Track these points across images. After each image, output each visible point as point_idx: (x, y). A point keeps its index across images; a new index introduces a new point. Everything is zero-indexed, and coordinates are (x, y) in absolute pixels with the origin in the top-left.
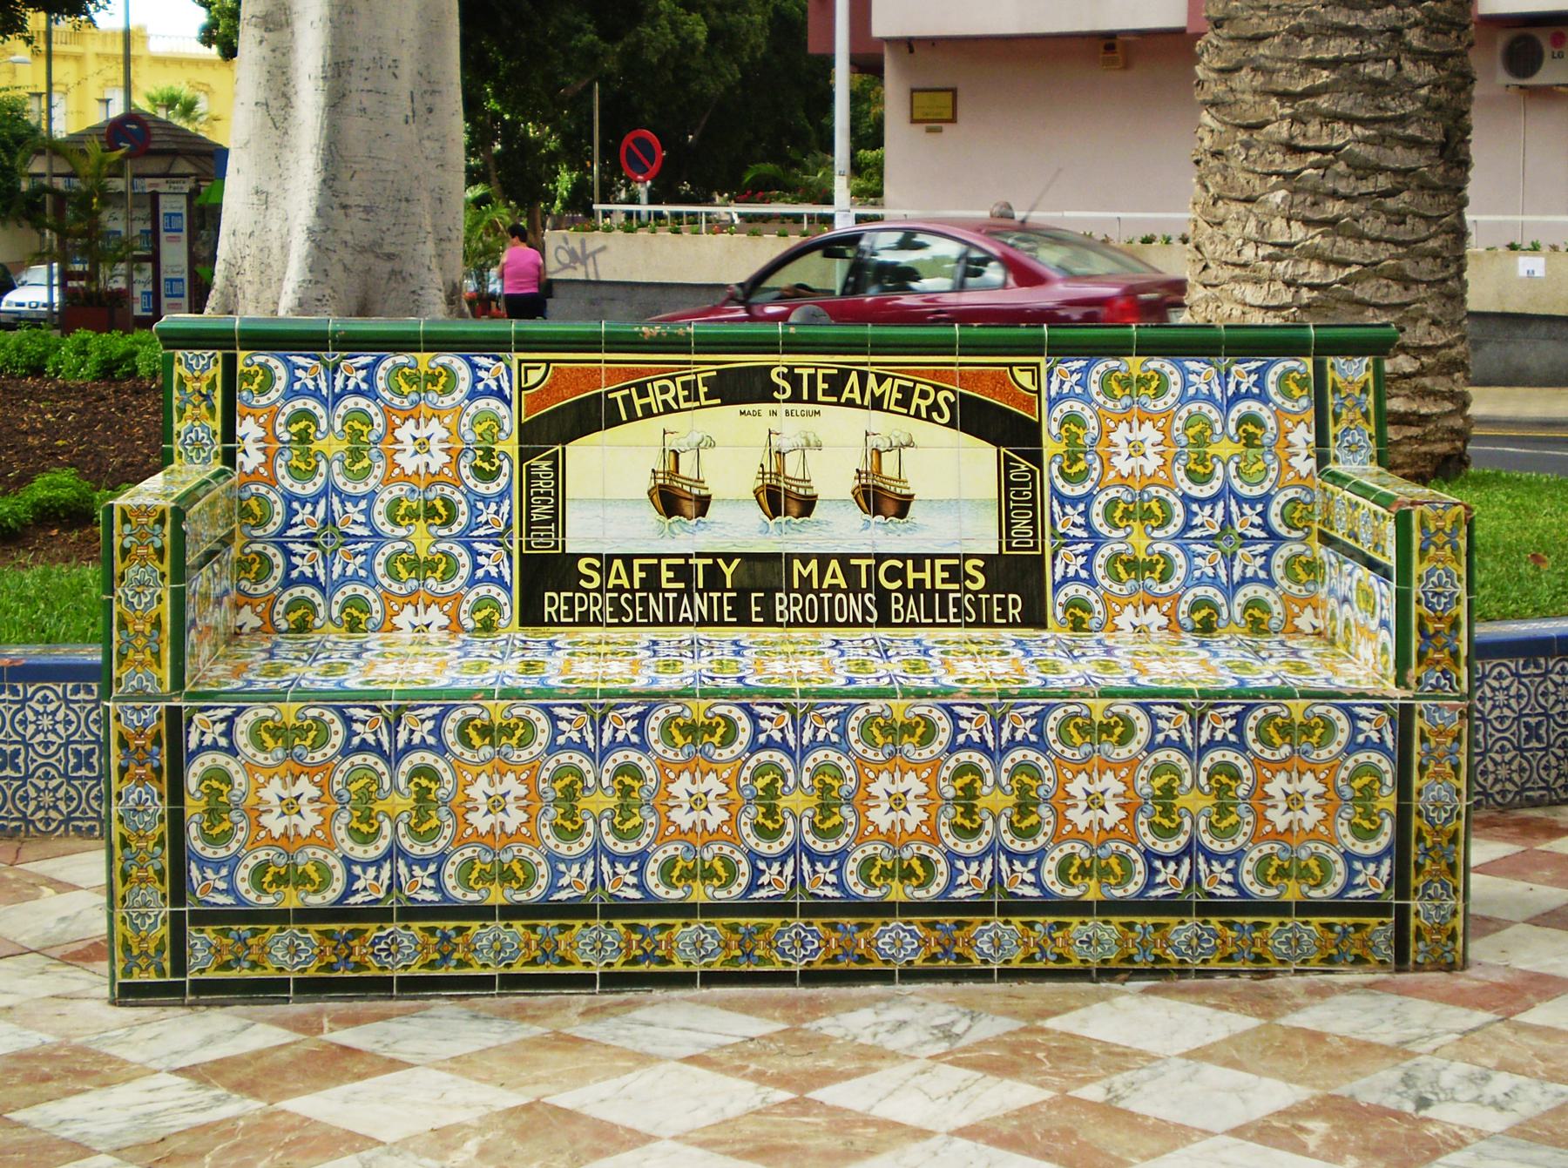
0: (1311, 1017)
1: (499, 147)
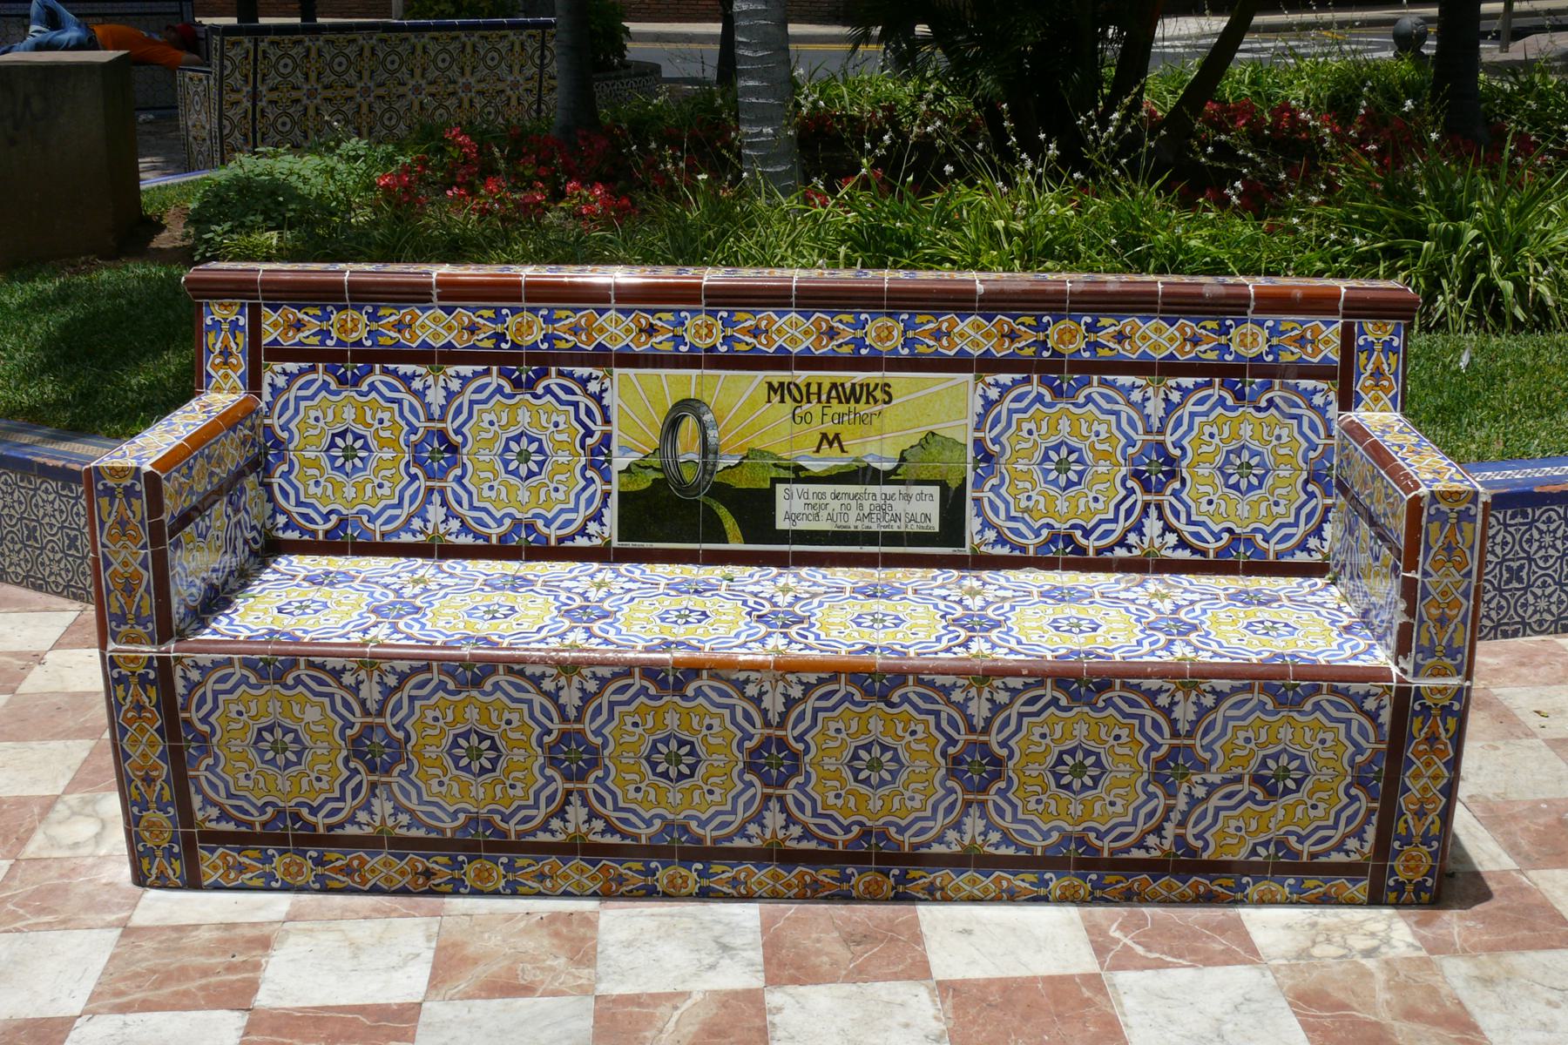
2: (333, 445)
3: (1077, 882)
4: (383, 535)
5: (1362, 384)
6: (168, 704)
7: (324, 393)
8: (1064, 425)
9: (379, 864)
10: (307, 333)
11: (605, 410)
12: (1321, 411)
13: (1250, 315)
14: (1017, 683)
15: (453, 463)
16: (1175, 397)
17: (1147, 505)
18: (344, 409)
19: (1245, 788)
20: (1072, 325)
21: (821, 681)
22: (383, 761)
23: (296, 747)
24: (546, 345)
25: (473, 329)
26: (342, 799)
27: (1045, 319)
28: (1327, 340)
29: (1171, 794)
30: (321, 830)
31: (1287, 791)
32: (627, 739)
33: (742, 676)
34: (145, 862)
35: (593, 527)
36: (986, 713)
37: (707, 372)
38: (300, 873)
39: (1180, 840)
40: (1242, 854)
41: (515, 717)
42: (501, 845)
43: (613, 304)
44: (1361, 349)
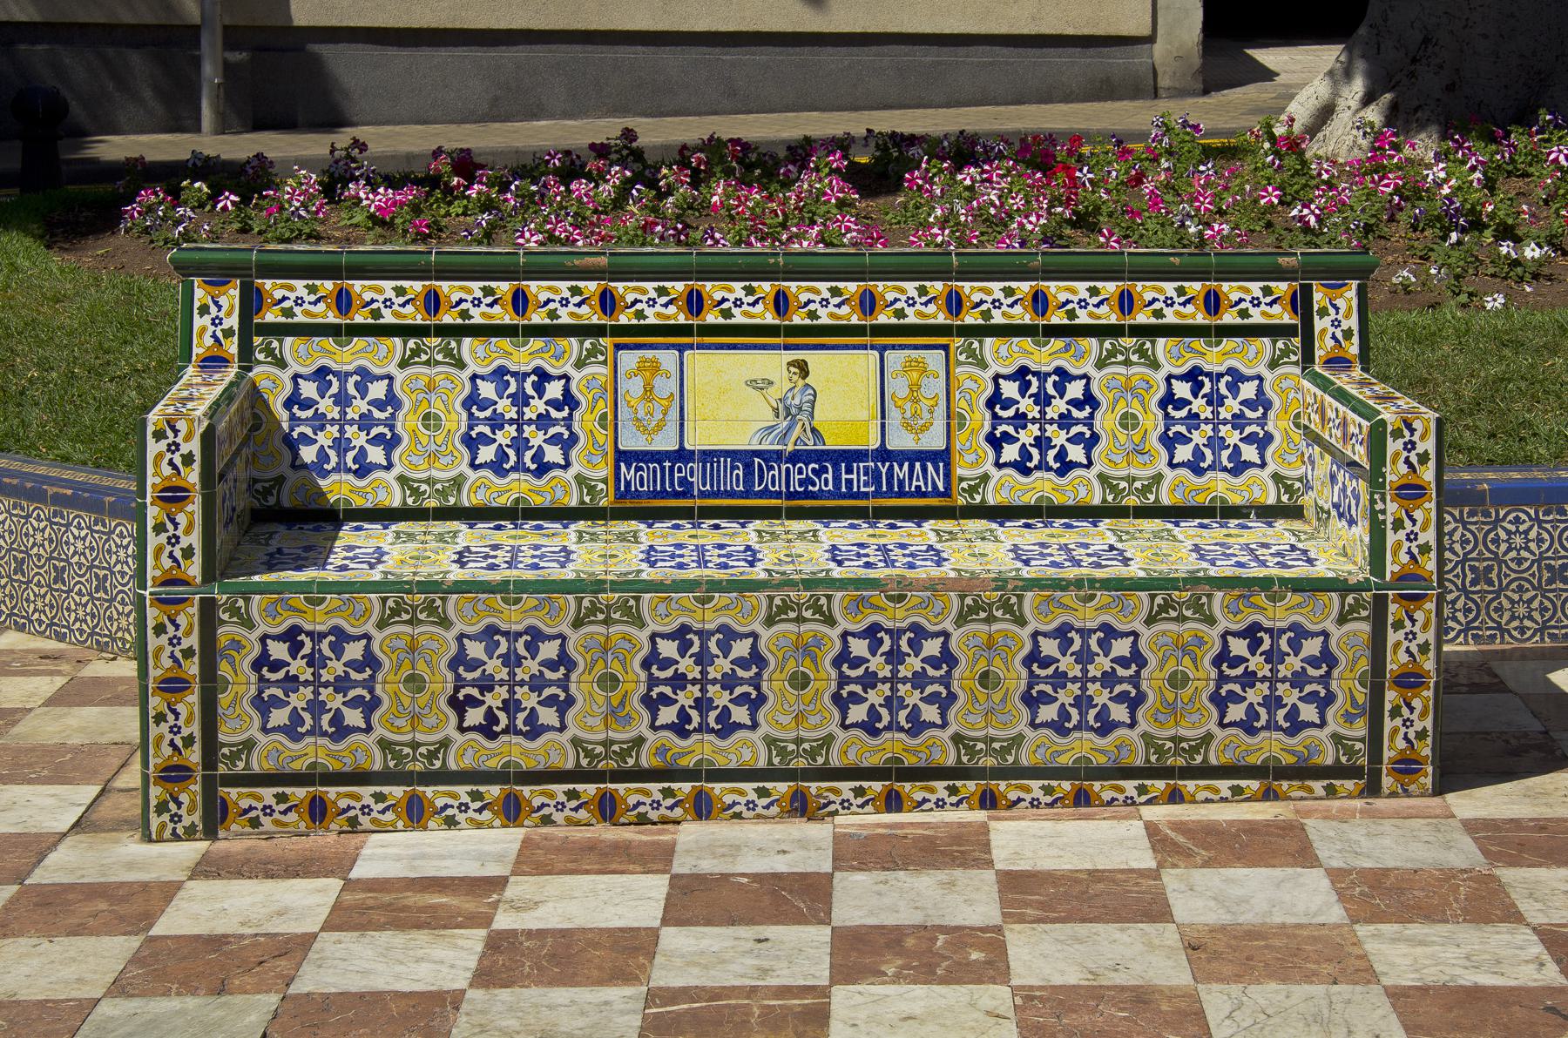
0: (1229, 917)
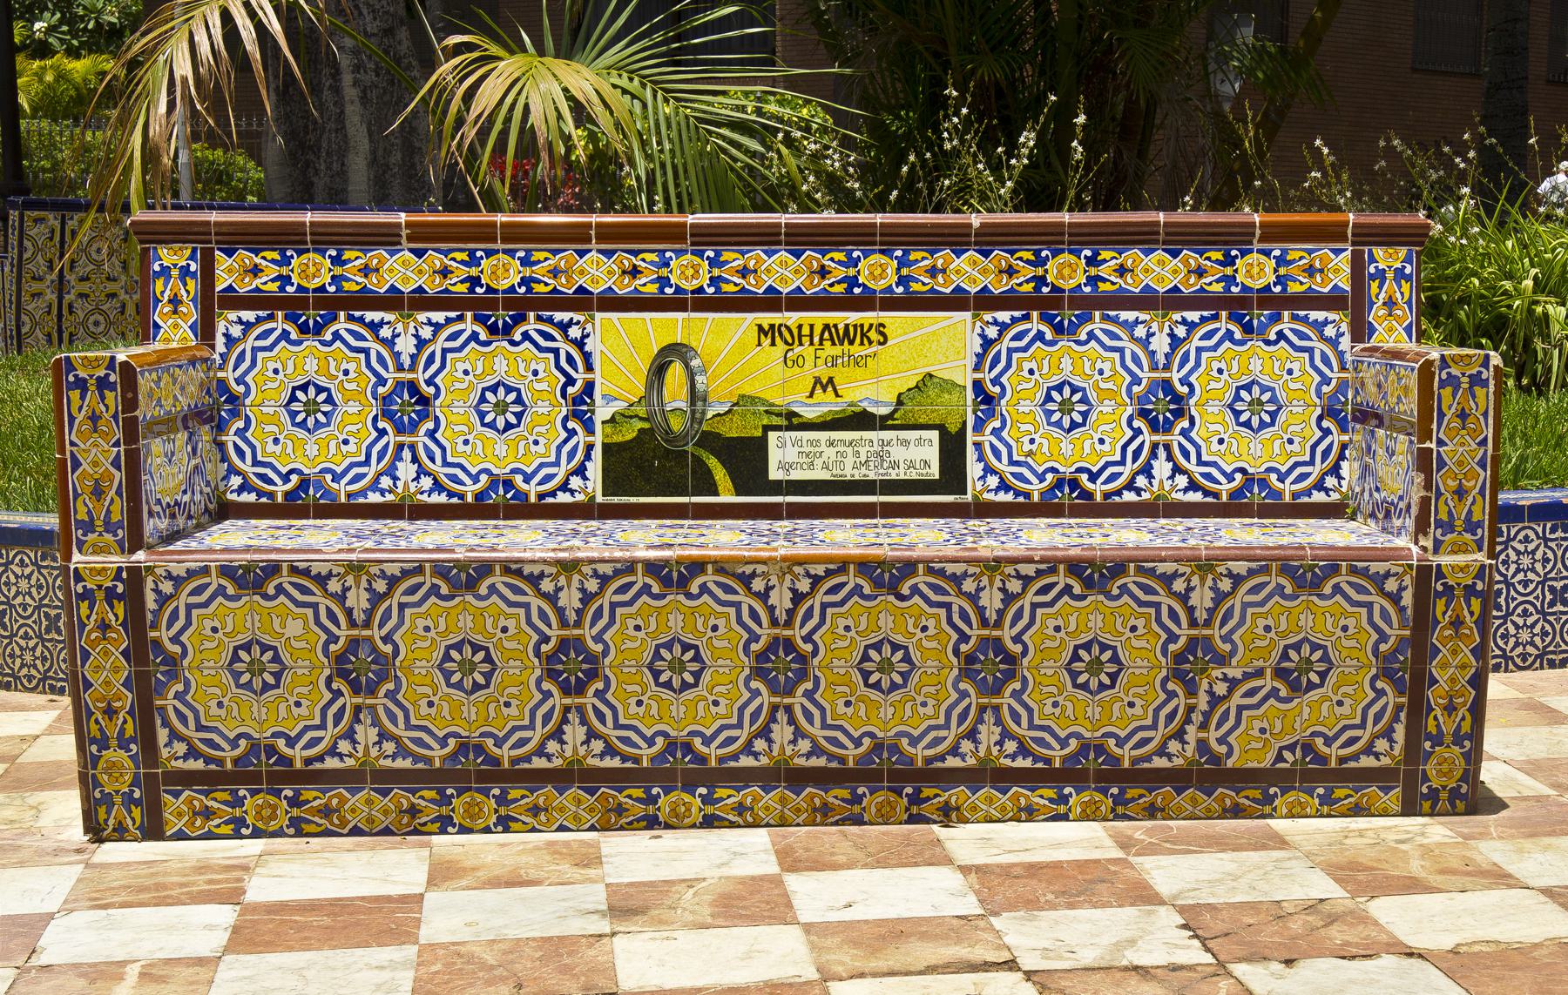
1: (1466, 136)
2: (293, 399)
3: (1098, 796)
4: (349, 496)
5: (1376, 314)
6: (136, 622)
7: (283, 343)
8: (1066, 363)
9: (358, 803)
10: (265, 279)
11: (587, 357)
12: (1333, 342)
13: (1256, 246)
14: (1029, 570)
15: (423, 416)
16: (1181, 331)
17: (1155, 446)
18: (306, 360)
19: (1268, 682)
20: (1073, 259)
21: (829, 573)
22: (368, 679)
23: (275, 667)
24: (523, 289)
25: (445, 272)
26: (323, 726)
27: (1044, 254)
28: (1337, 270)
29: (1192, 691)
30: (298, 765)
31: (1311, 686)
32: (629, 644)
33: (748, 569)
34: (102, 811)
35: (575, 482)
36: (998, 605)
37: (693, 315)
38: (273, 817)
39: (1202, 746)
40: (1267, 763)
41: (511, 624)
42: (493, 775)
43: (594, 245)
44: (1372, 277)
